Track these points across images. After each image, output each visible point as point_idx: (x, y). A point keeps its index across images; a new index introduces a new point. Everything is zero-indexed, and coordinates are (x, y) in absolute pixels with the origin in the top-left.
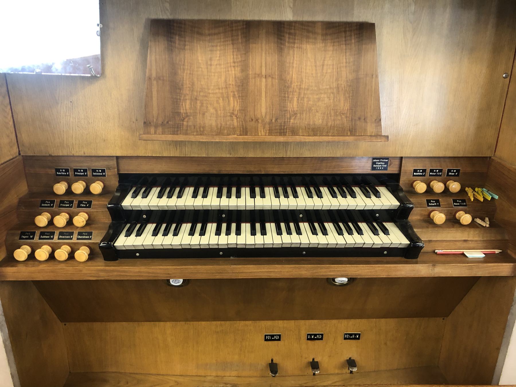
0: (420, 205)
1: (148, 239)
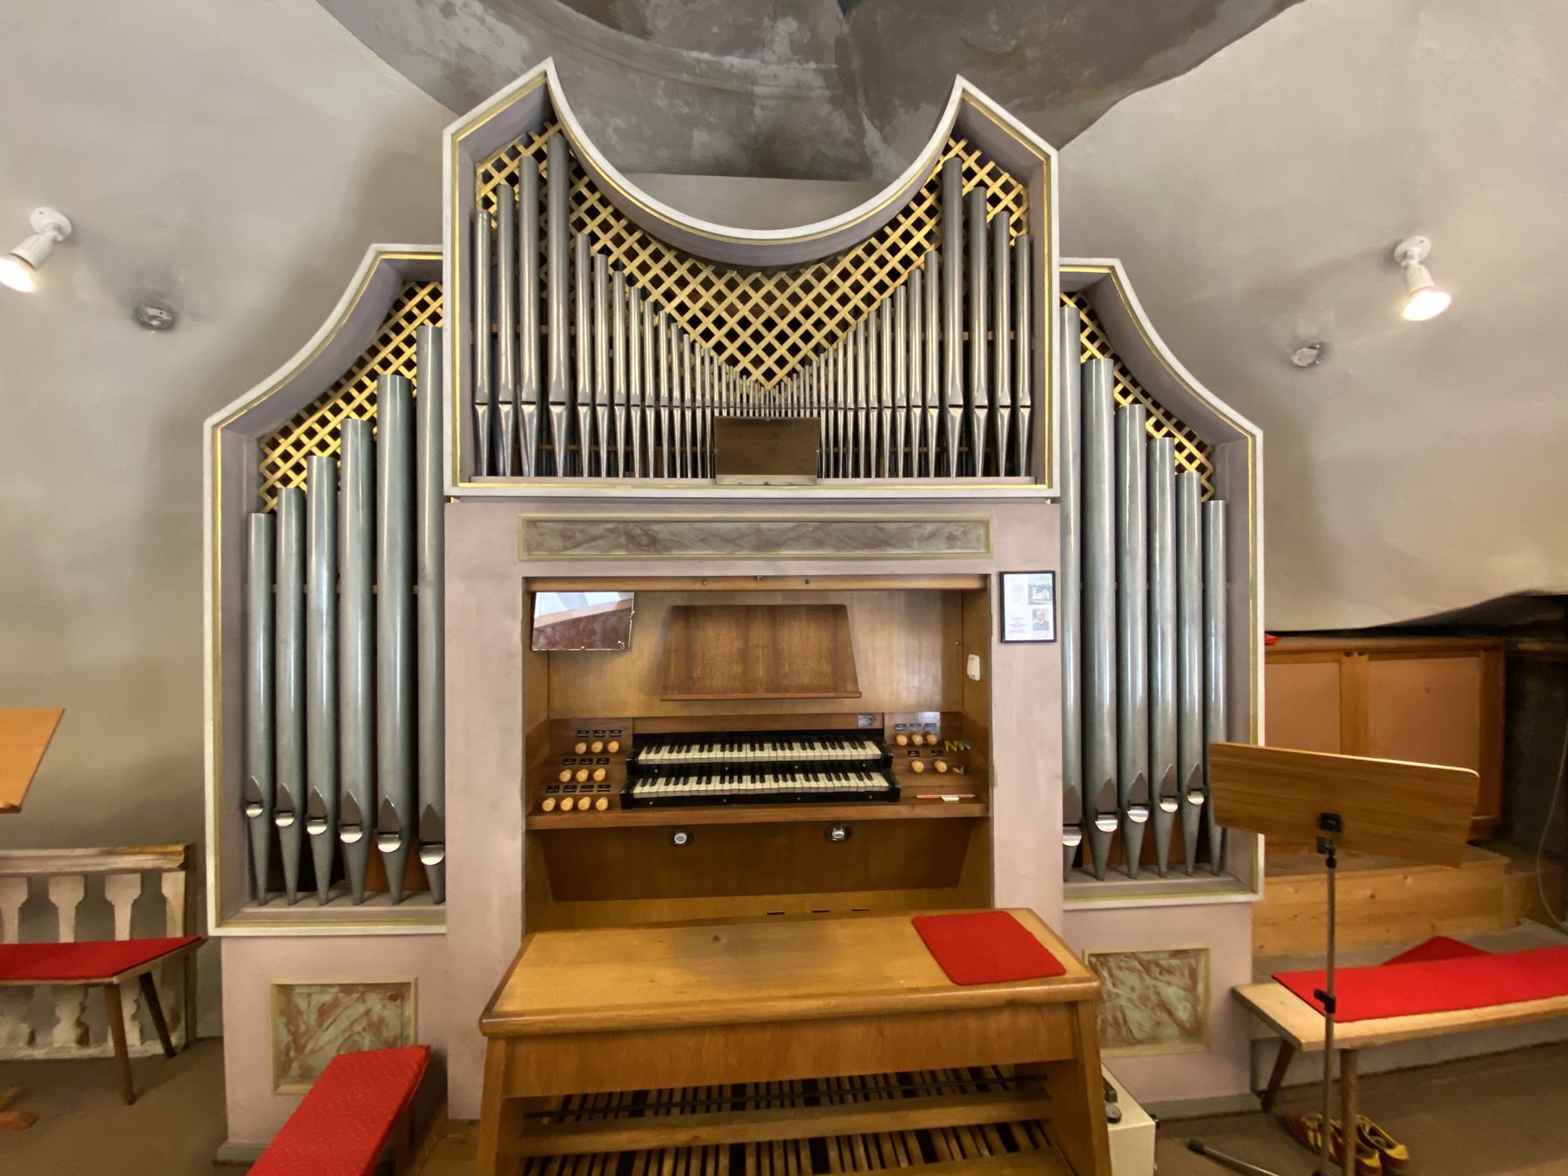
0: (902, 756)
1: (661, 788)
